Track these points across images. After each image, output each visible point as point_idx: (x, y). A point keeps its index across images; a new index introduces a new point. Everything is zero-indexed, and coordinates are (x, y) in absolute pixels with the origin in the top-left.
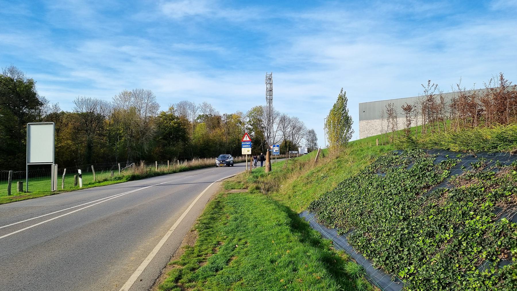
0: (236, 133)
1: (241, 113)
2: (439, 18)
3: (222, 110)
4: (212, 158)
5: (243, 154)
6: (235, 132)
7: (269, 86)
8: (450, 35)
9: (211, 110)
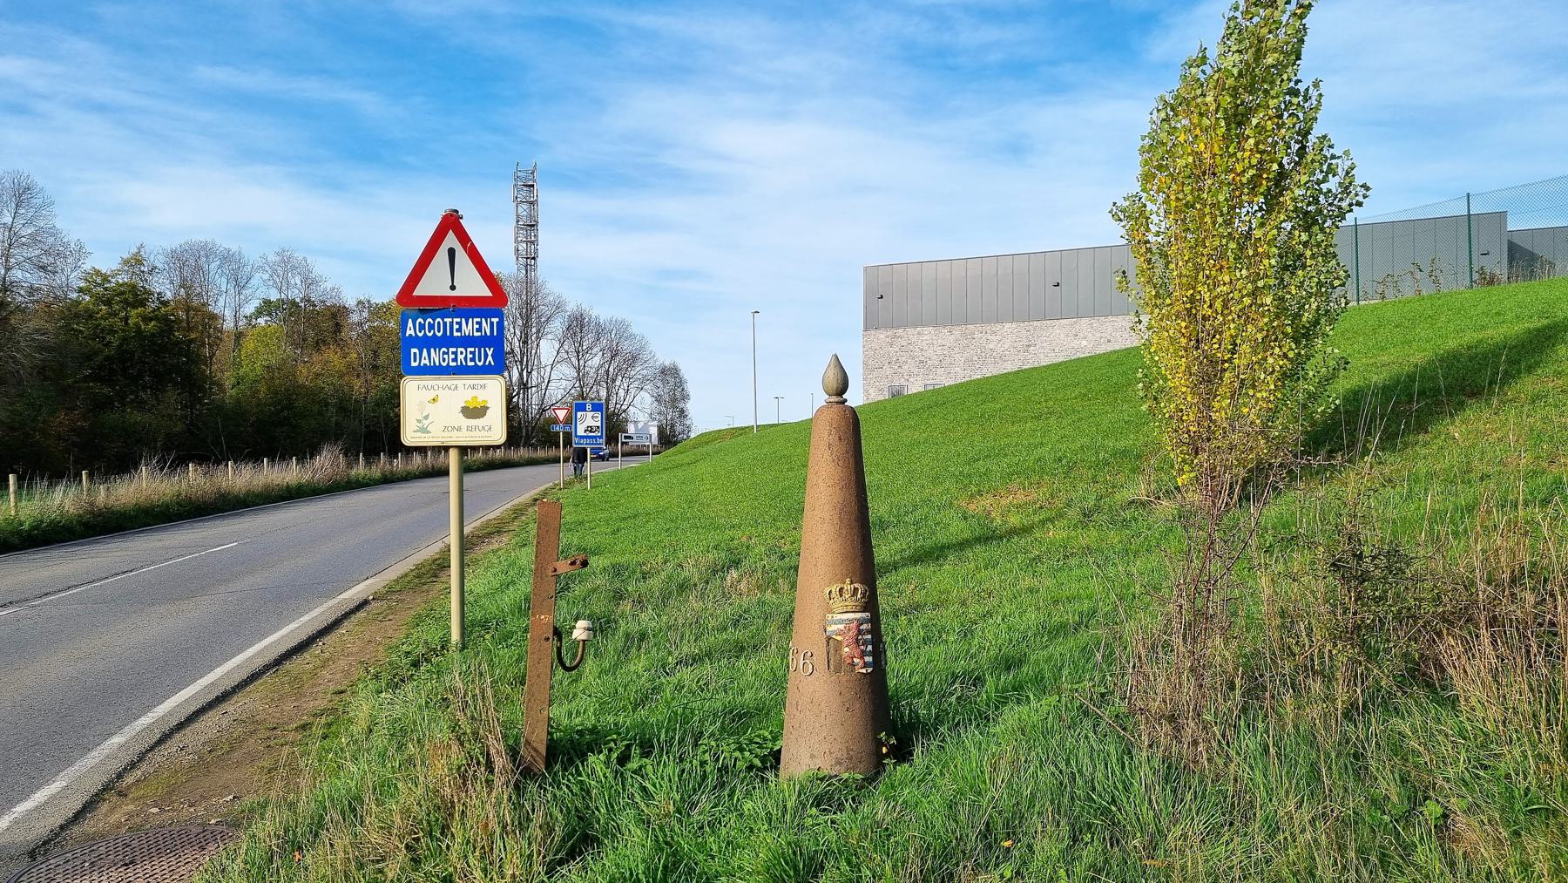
2: (1019, 70)
4: (272, 460)
5: (409, 437)
8: (1044, 118)
9: (309, 282)
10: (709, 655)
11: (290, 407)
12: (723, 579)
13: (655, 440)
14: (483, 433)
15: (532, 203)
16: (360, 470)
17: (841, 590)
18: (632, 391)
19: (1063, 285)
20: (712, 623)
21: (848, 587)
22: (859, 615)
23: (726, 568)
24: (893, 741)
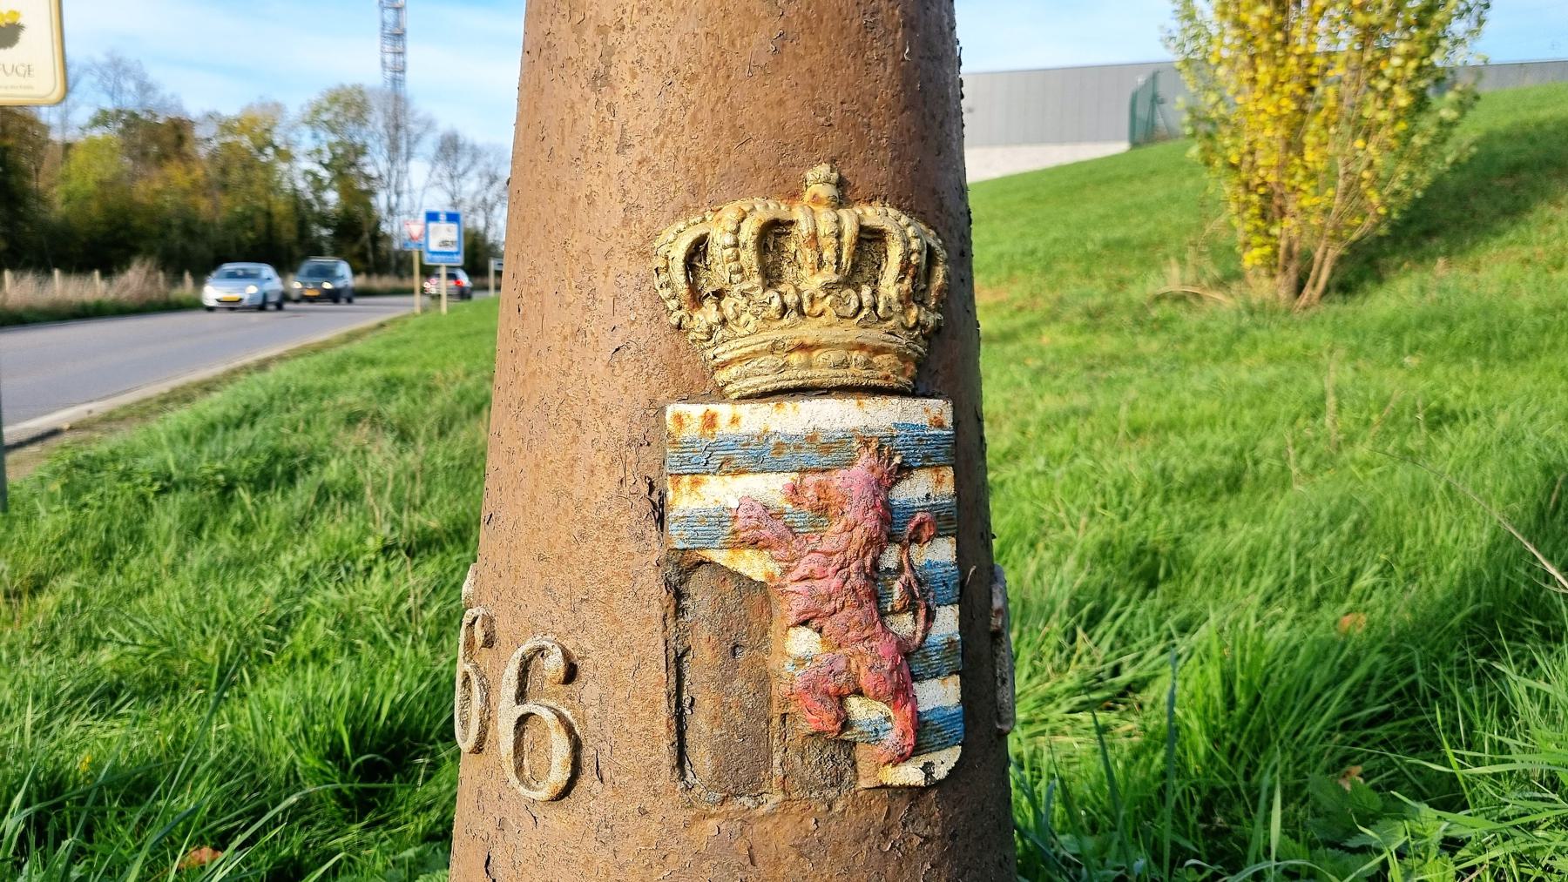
0: (255, 188)
1: (278, 107)
3: (204, 96)
5: (957, 678)
6: (250, 182)
7: (389, 15)
9: (145, 88)
11: (127, 227)
14: (14, 80)
15: (398, 9)
16: (345, 348)
17: (773, 233)
21: (817, 220)
22: (884, 414)
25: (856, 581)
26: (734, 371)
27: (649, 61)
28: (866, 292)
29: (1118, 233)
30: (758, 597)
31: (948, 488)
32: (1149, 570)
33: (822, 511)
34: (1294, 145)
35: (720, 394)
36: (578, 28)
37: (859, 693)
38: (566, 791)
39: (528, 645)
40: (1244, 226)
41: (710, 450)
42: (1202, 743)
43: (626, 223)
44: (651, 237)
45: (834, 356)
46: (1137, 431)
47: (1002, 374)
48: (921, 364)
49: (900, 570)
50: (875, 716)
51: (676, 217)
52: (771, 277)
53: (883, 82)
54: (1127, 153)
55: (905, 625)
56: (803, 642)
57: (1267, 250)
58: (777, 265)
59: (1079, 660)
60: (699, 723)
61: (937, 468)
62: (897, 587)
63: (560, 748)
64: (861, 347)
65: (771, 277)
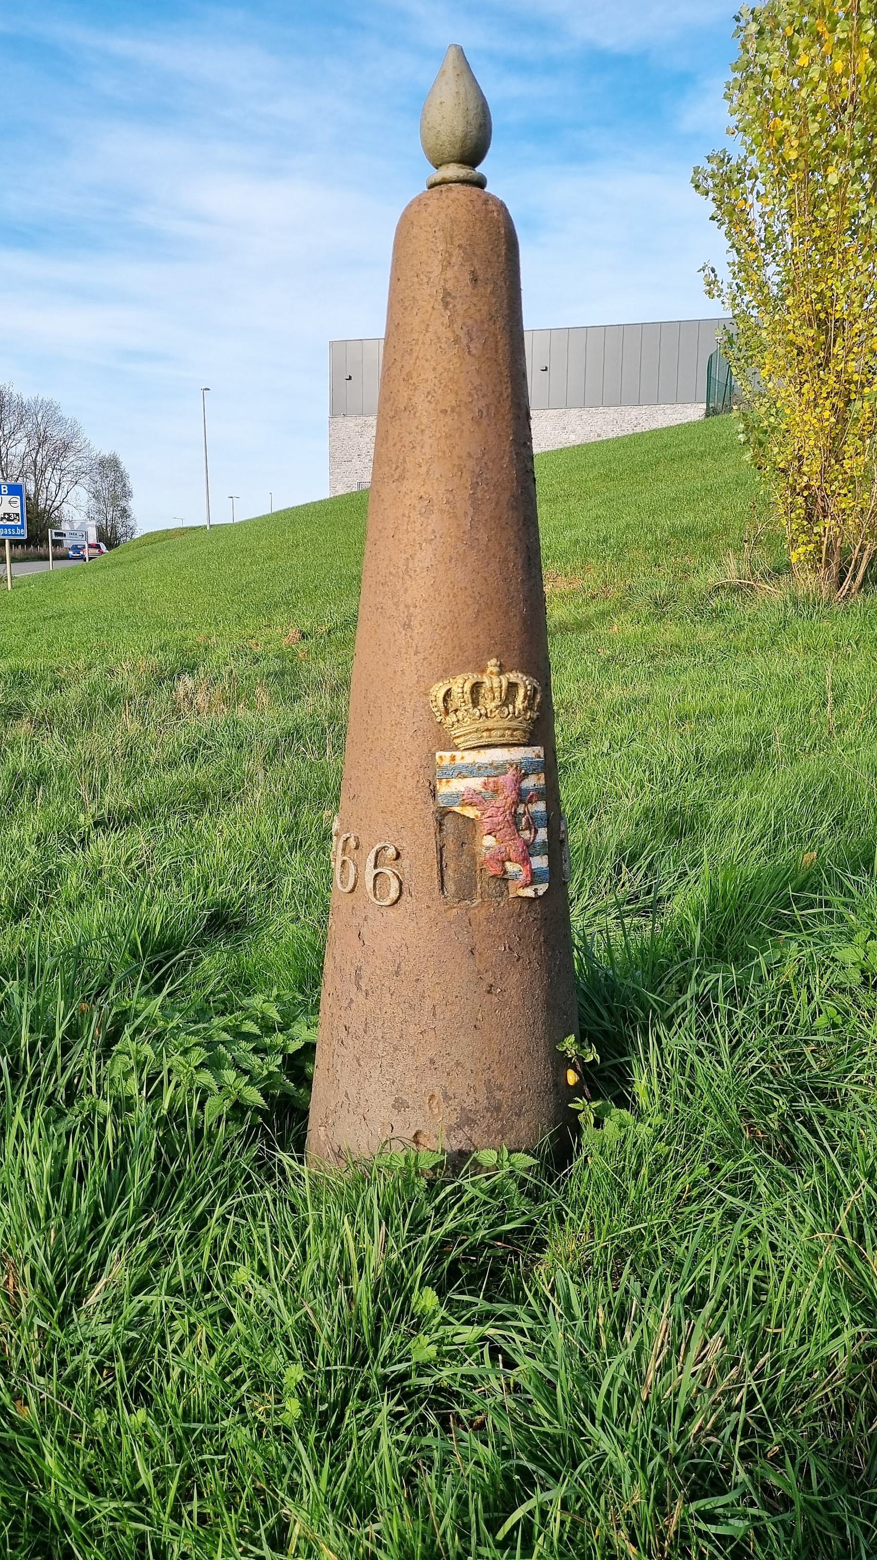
10: (148, 810)
12: (172, 689)
13: (93, 539)
17: (476, 687)
18: (65, 485)
19: (552, 369)
20: (155, 755)
21: (494, 682)
22: (518, 754)
23: (174, 675)
24: (592, 1055)
25: (509, 818)
26: (462, 739)
27: (427, 620)
28: (511, 707)
29: (687, 519)
30: (471, 824)
31: (542, 782)
32: (680, 826)
33: (495, 792)
34: (835, 453)
35: (456, 748)
36: (396, 604)
37: (510, 860)
38: (396, 902)
39: (378, 846)
40: (789, 526)
41: (454, 769)
42: (697, 935)
43: (418, 682)
44: (428, 688)
45: (499, 733)
46: (683, 718)
47: (576, 665)
48: (531, 733)
49: (525, 813)
50: (516, 869)
51: (438, 681)
52: (475, 703)
53: (516, 625)
54: (699, 422)
55: (527, 835)
56: (489, 841)
57: (811, 547)
58: (477, 698)
59: (623, 885)
60: (449, 872)
61: (538, 774)
62: (524, 820)
63: (395, 884)
64: (509, 729)
65: (475, 703)
